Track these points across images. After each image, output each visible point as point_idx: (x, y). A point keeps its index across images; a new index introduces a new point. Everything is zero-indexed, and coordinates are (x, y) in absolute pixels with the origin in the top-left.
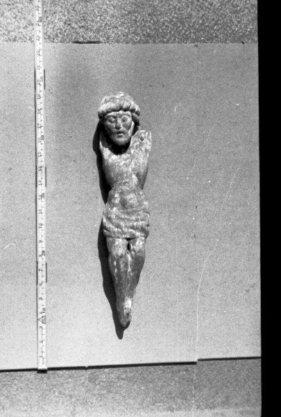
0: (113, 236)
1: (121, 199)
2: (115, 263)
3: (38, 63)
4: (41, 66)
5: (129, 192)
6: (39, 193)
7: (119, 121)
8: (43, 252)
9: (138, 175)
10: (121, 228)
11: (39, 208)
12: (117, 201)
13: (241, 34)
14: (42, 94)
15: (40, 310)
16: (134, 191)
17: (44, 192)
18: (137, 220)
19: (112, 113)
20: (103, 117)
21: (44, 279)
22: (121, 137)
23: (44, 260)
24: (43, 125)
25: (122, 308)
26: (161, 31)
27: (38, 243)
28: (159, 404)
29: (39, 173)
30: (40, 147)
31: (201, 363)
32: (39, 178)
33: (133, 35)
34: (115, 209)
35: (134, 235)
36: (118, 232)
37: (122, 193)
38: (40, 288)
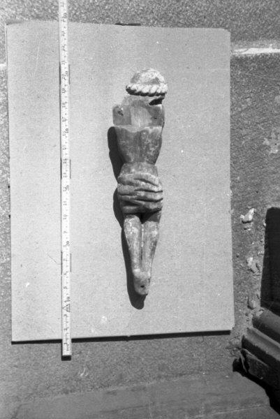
3: (62, 58)
6: (64, 185)
8: (68, 242)
11: (64, 199)
13: (133, 13)
14: (66, 88)
17: (68, 184)
21: (68, 269)
23: (68, 250)
26: (50, 11)
28: (53, 388)
29: (64, 165)
32: (64, 171)
33: (21, 16)
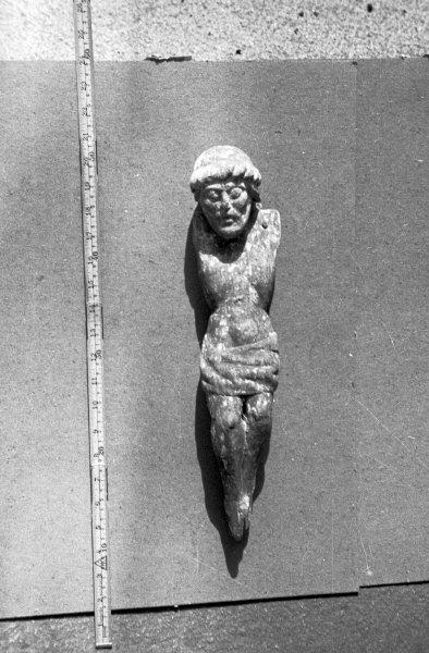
0: (218, 391)
1: (231, 328)
2: (222, 438)
4: (91, 134)
5: (244, 317)
7: (226, 197)
8: (101, 449)
9: (258, 287)
10: (231, 378)
12: (224, 333)
15: (98, 547)
16: (252, 315)
17: (99, 348)
18: (258, 364)
19: (217, 186)
20: (199, 190)
21: (103, 495)
22: (230, 224)
24: (95, 234)
25: (236, 509)
27: (92, 434)
30: (98, 464)
31: (367, 591)
34: (220, 346)
35: (253, 389)
36: (227, 385)
37: (232, 319)
38: (97, 510)
